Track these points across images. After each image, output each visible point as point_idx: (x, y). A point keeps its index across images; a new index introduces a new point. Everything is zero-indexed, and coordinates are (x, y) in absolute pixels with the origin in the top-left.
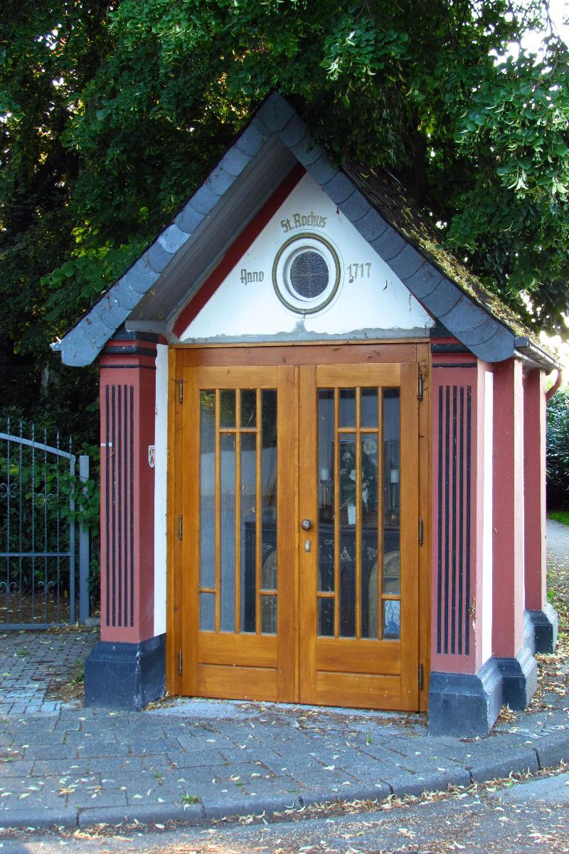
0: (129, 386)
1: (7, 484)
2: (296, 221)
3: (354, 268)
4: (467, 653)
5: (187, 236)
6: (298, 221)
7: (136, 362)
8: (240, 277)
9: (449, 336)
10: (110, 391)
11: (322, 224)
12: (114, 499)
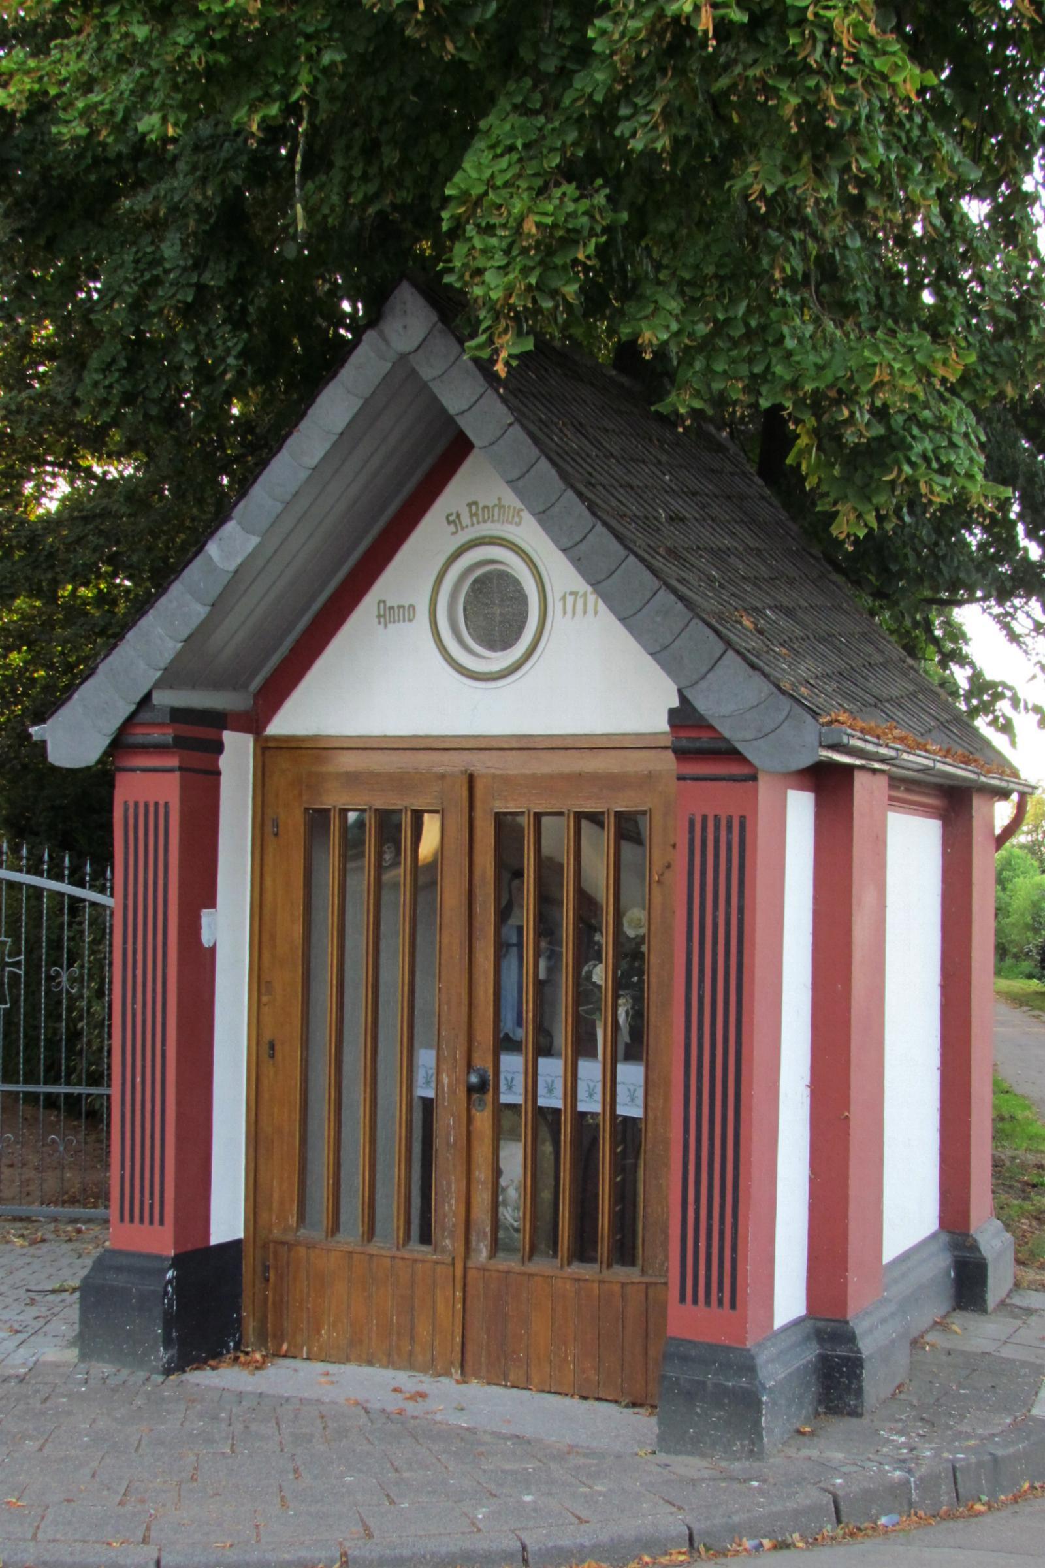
0: (162, 803)
1: (62, 967)
2: (472, 515)
3: (570, 600)
4: (733, 1306)
5: (255, 540)
6: (476, 514)
7: (174, 762)
8: (376, 613)
9: (703, 724)
10: (131, 811)
11: (517, 519)
12: (134, 1002)
